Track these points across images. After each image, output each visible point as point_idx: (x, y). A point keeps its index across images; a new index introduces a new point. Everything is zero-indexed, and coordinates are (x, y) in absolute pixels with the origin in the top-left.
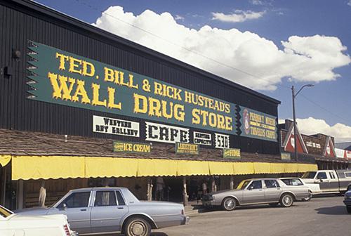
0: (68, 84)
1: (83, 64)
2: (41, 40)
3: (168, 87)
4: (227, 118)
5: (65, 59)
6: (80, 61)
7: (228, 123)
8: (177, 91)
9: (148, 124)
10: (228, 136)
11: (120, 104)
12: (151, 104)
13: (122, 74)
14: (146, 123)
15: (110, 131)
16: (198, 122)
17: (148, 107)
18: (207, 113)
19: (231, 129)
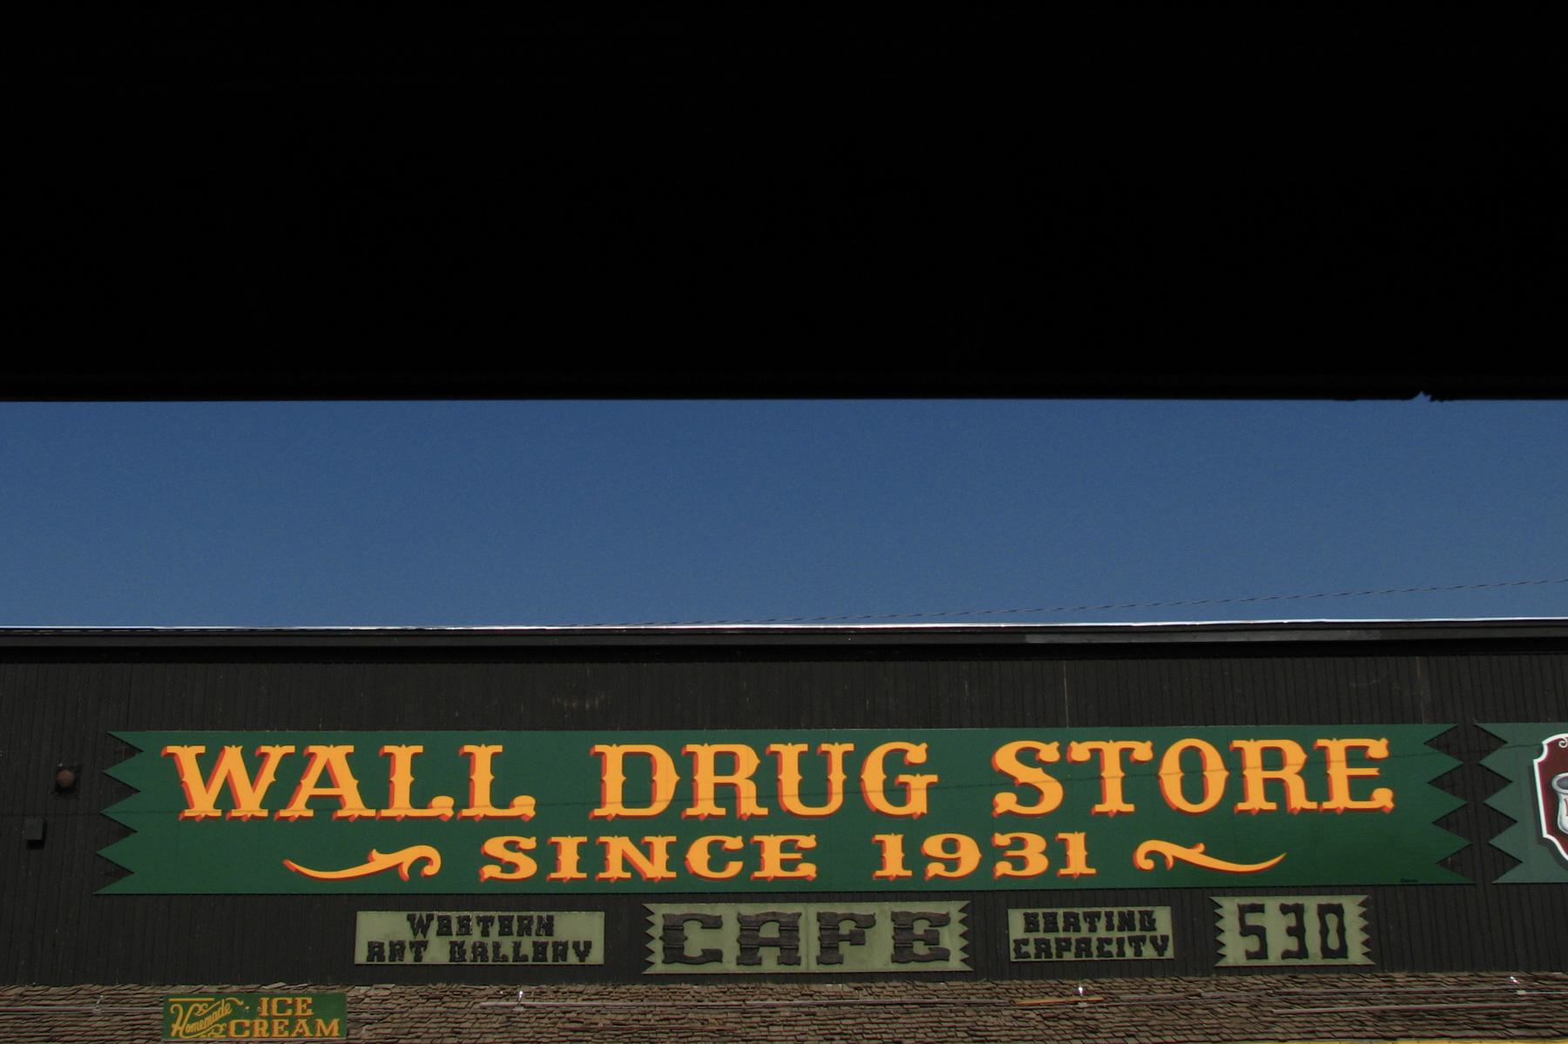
9: (660, 913)
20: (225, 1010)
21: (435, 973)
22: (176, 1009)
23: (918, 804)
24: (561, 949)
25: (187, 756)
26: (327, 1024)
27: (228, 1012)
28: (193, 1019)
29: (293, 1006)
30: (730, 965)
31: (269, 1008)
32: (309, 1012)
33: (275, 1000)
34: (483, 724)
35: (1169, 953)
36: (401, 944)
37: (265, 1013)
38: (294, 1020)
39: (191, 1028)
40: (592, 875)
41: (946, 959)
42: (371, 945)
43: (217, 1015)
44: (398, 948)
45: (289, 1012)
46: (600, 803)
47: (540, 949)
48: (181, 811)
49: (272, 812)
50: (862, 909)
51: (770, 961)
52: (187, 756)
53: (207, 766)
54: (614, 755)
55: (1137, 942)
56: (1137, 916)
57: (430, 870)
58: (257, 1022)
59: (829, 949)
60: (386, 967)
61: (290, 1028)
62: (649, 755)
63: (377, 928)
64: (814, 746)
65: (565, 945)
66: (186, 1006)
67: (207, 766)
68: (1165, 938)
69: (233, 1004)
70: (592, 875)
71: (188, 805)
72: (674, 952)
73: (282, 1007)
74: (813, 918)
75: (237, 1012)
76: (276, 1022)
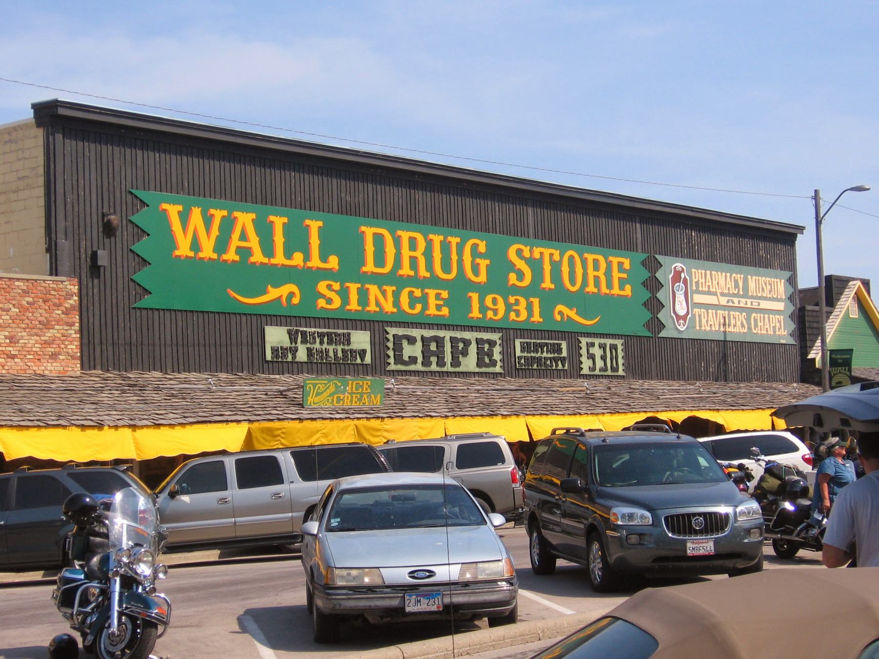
9: (392, 331)
10: (619, 343)
20: (332, 389)
22: (310, 388)
23: (483, 278)
25: (174, 210)
27: (333, 390)
28: (318, 394)
29: (362, 387)
30: (419, 367)
32: (369, 391)
34: (312, 206)
35: (368, 359)
38: (362, 394)
39: (317, 399)
40: (364, 308)
41: (495, 365)
43: (329, 392)
46: (365, 265)
48: (360, 268)
49: (219, 255)
51: (470, 363)
52: (174, 210)
53: (185, 218)
54: (369, 232)
56: (447, 339)
57: (296, 300)
60: (282, 362)
61: (360, 400)
62: (383, 235)
63: (276, 336)
64: (445, 238)
66: (315, 385)
67: (185, 218)
70: (364, 308)
71: (177, 248)
72: (399, 359)
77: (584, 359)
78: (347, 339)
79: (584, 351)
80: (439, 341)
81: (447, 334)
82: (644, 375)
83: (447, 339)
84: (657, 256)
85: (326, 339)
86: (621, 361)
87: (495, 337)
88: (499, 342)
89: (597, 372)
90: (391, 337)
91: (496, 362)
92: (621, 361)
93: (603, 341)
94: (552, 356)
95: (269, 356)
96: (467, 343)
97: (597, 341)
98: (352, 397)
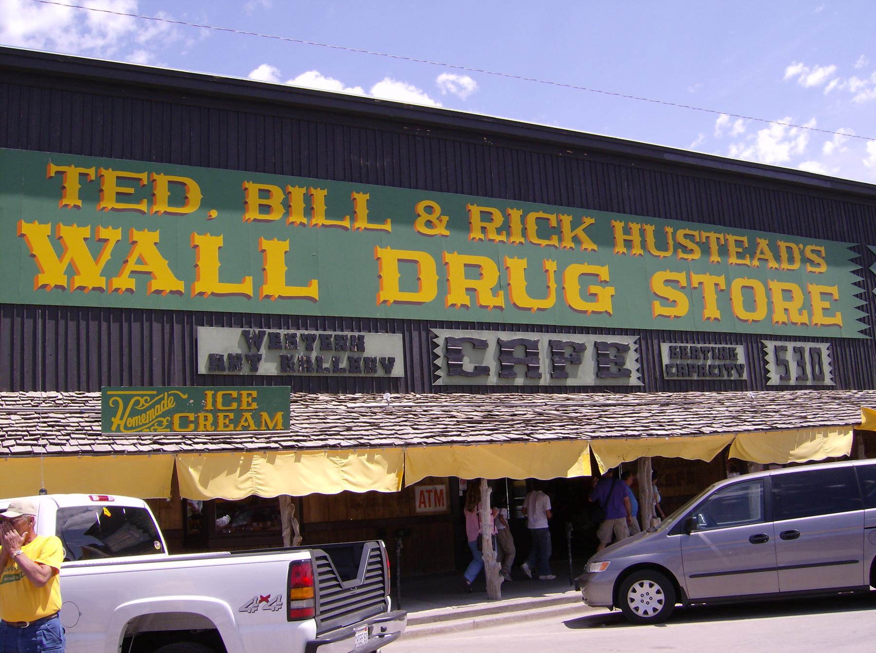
0: (96, 244)
1: (726, 240)
2: (627, 209)
3: (532, 217)
4: (815, 290)
5: (718, 239)
6: (144, 176)
7: (818, 304)
8: (574, 226)
9: (442, 335)
10: (824, 347)
11: (315, 283)
12: (777, 297)
13: (650, 229)
14: (435, 331)
15: (268, 367)
16: (682, 309)
17: (770, 303)
18: (721, 281)
19: (838, 319)
20: (168, 403)
21: (269, 380)
22: (116, 403)
24: (371, 363)
26: (272, 419)
28: (134, 413)
29: (239, 400)
30: (493, 380)
31: (214, 402)
32: (255, 406)
33: (220, 394)
36: (238, 357)
37: (209, 407)
42: (212, 357)
43: (160, 409)
44: (235, 360)
45: (235, 406)
47: (353, 363)
50: (577, 339)
51: (586, 374)
55: (728, 369)
57: (834, 290)
58: (201, 415)
59: (557, 371)
60: (226, 374)
65: (374, 360)
66: (126, 399)
68: (741, 366)
69: (176, 397)
72: (455, 370)
73: (227, 400)
74: (546, 344)
75: (181, 406)
76: (221, 415)
77: (771, 366)
78: (360, 344)
79: (770, 357)
80: (530, 350)
81: (543, 339)
82: (846, 387)
83: (298, 335)
84: (869, 247)
85: (710, 355)
86: (827, 369)
87: (628, 341)
88: (633, 347)
89: (793, 382)
90: (440, 341)
91: (630, 372)
92: (827, 369)
93: (799, 344)
94: (722, 363)
95: (202, 369)
96: (579, 349)
97: (790, 345)
98: (216, 418)
